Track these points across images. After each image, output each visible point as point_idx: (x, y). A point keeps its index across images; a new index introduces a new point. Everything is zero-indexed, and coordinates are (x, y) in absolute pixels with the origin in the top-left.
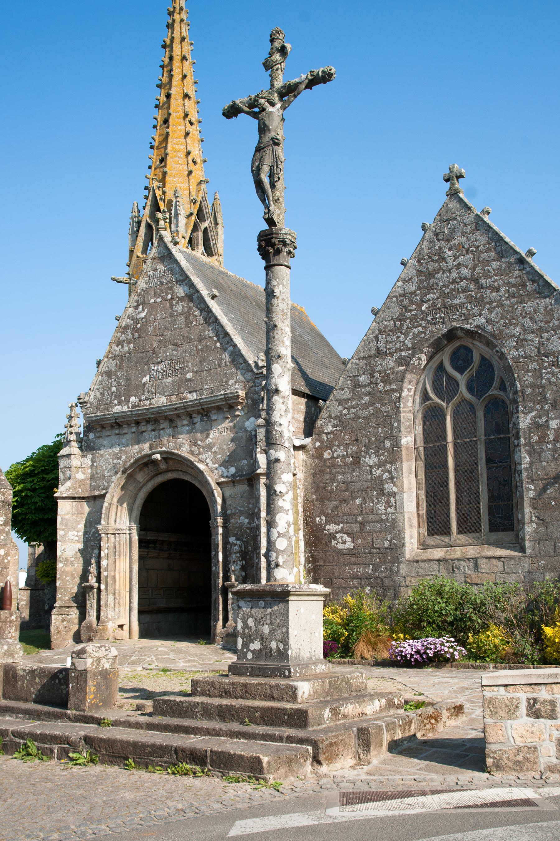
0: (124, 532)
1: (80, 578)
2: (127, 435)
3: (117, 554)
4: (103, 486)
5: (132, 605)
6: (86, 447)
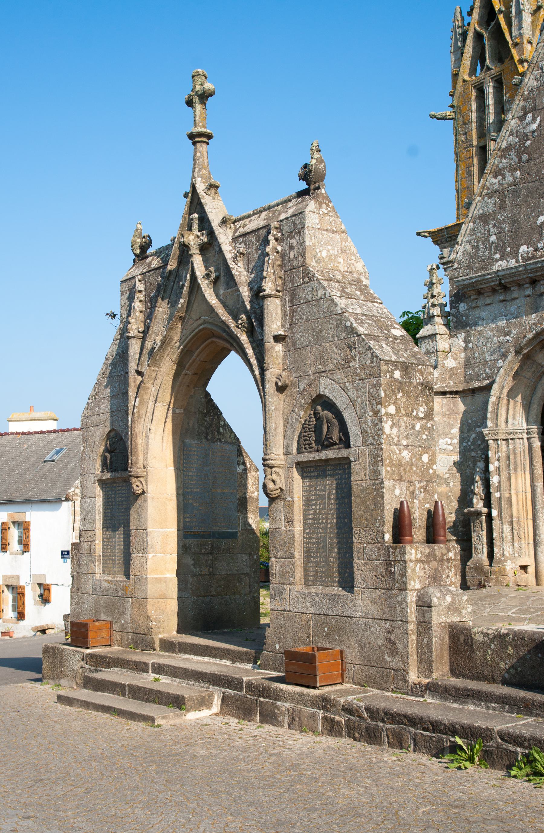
0: (520, 436)
1: (458, 501)
2: (517, 301)
3: (512, 467)
4: (484, 375)
5: (538, 538)
6: (456, 322)
